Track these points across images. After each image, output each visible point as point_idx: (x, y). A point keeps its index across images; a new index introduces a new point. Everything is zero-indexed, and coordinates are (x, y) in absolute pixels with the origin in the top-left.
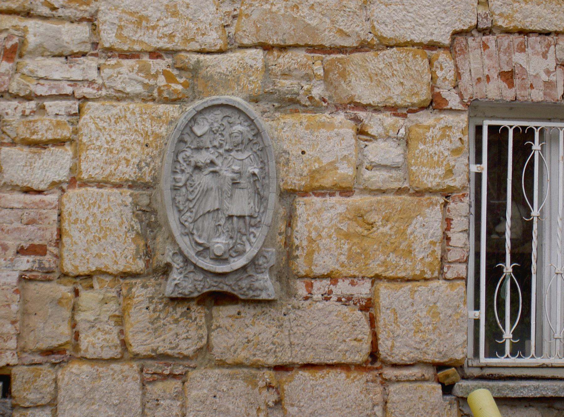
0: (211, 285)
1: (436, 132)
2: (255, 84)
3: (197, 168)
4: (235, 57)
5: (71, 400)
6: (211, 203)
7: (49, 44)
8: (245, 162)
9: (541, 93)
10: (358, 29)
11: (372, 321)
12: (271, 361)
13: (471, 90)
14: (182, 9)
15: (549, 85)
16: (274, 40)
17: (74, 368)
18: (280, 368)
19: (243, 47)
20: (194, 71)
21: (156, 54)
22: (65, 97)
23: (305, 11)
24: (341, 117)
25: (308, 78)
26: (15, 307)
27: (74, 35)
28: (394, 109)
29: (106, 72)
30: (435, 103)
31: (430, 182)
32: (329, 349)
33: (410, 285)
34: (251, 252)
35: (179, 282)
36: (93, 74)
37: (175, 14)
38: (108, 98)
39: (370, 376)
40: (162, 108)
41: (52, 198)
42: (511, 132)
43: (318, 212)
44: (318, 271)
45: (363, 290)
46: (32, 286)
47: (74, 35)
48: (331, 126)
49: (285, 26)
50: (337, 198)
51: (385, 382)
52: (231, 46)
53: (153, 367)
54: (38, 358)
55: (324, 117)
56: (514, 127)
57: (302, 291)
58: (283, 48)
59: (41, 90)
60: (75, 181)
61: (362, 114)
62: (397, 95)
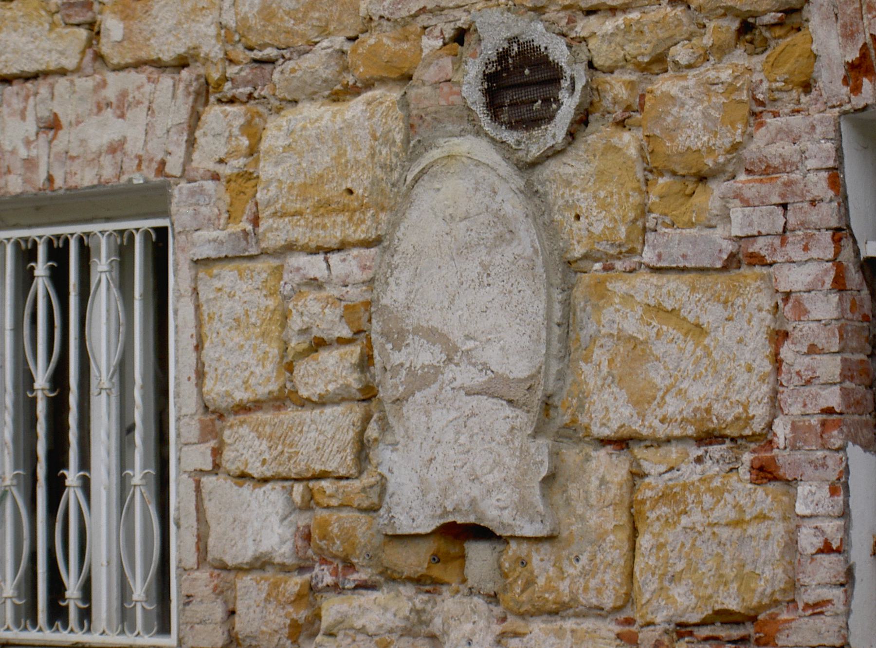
9: (20, 180)
15: (30, 164)
42: (138, 238)
56: (12, 240)
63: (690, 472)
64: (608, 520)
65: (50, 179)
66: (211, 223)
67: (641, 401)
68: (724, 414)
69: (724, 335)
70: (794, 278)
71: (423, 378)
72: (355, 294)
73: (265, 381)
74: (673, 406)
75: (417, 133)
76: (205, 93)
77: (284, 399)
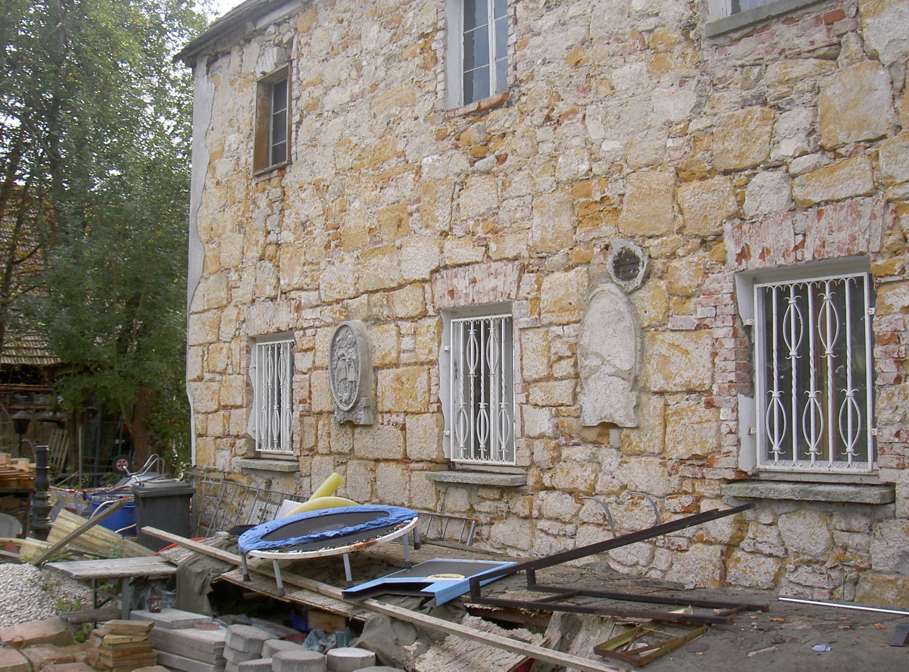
1: (424, 329)
10: (397, 279)
15: (467, 295)
18: (377, 461)
27: (312, 296)
32: (390, 451)
33: (417, 416)
42: (809, 287)
45: (400, 419)
57: (380, 421)
61: (399, 323)
64: (657, 421)
65: (473, 300)
66: (525, 315)
67: (667, 378)
68: (695, 382)
69: (695, 354)
70: (719, 333)
73: (543, 373)
74: (678, 380)
75: (592, 283)
77: (549, 378)
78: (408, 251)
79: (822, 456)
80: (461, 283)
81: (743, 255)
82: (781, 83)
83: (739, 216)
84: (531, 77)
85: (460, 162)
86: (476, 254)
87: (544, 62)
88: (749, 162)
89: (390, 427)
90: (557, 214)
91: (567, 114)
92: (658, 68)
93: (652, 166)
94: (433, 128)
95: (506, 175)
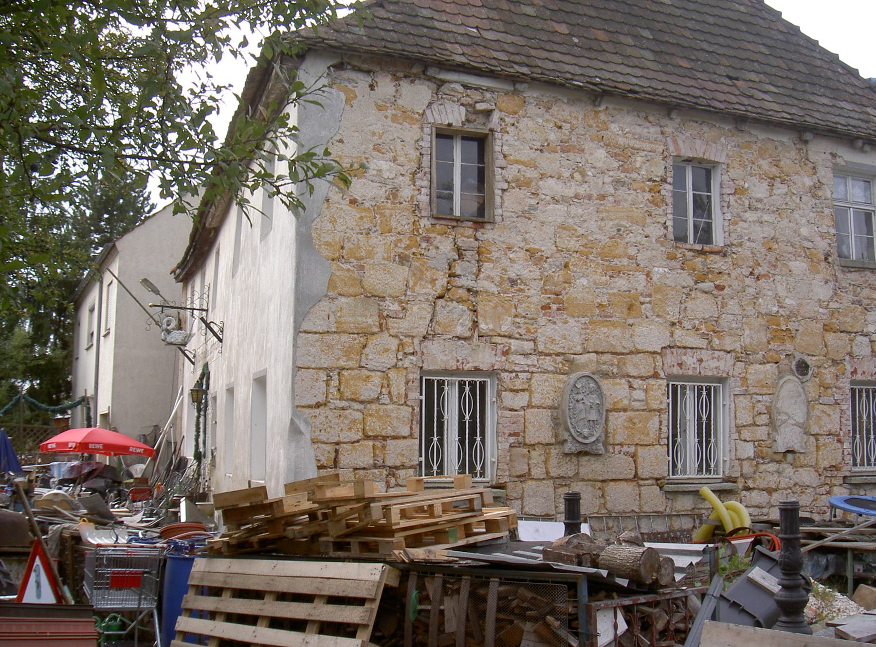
0: (580, 448)
1: (656, 387)
2: (593, 367)
3: (578, 401)
4: (587, 355)
5: (529, 496)
6: (583, 415)
7: (520, 350)
8: (594, 399)
10: (629, 346)
11: (635, 461)
12: (601, 478)
13: (668, 370)
14: (567, 337)
15: (694, 368)
16: (600, 350)
17: (530, 483)
18: (603, 481)
19: (589, 352)
20: (571, 362)
21: (558, 354)
22: (525, 371)
23: (611, 338)
24: (623, 381)
25: (612, 365)
26: (508, 458)
27: (528, 346)
28: (641, 378)
29: (541, 361)
30: (656, 376)
31: (655, 407)
32: (621, 473)
34: (597, 435)
35: (569, 447)
36: (535, 363)
37: (565, 339)
38: (541, 372)
39: (635, 483)
40: (561, 376)
41: (522, 413)
43: (616, 419)
44: (617, 442)
45: (632, 449)
46: (514, 449)
47: (528, 346)
48: (621, 384)
49: (604, 344)
50: (622, 413)
51: (640, 486)
52: (586, 351)
53: (558, 481)
54: (516, 479)
55: (618, 380)
58: (602, 353)
59: (517, 369)
60: (530, 406)
62: (644, 373)
63: (827, 441)
64: (813, 449)
65: (700, 373)
66: (739, 387)
67: (820, 428)
68: (833, 430)
69: (833, 416)
70: (844, 407)
71: (785, 422)
72: (768, 404)
75: (781, 374)
76: (738, 360)
77: (754, 424)
78: (638, 330)
79: (862, 464)
80: (690, 360)
81: (854, 372)
82: (868, 298)
83: (850, 354)
84: (740, 245)
85: (687, 280)
86: (703, 343)
87: (749, 239)
88: (855, 330)
89: (622, 456)
90: (759, 331)
91: (764, 276)
92: (814, 270)
93: (813, 319)
94: (663, 249)
95: (723, 299)
